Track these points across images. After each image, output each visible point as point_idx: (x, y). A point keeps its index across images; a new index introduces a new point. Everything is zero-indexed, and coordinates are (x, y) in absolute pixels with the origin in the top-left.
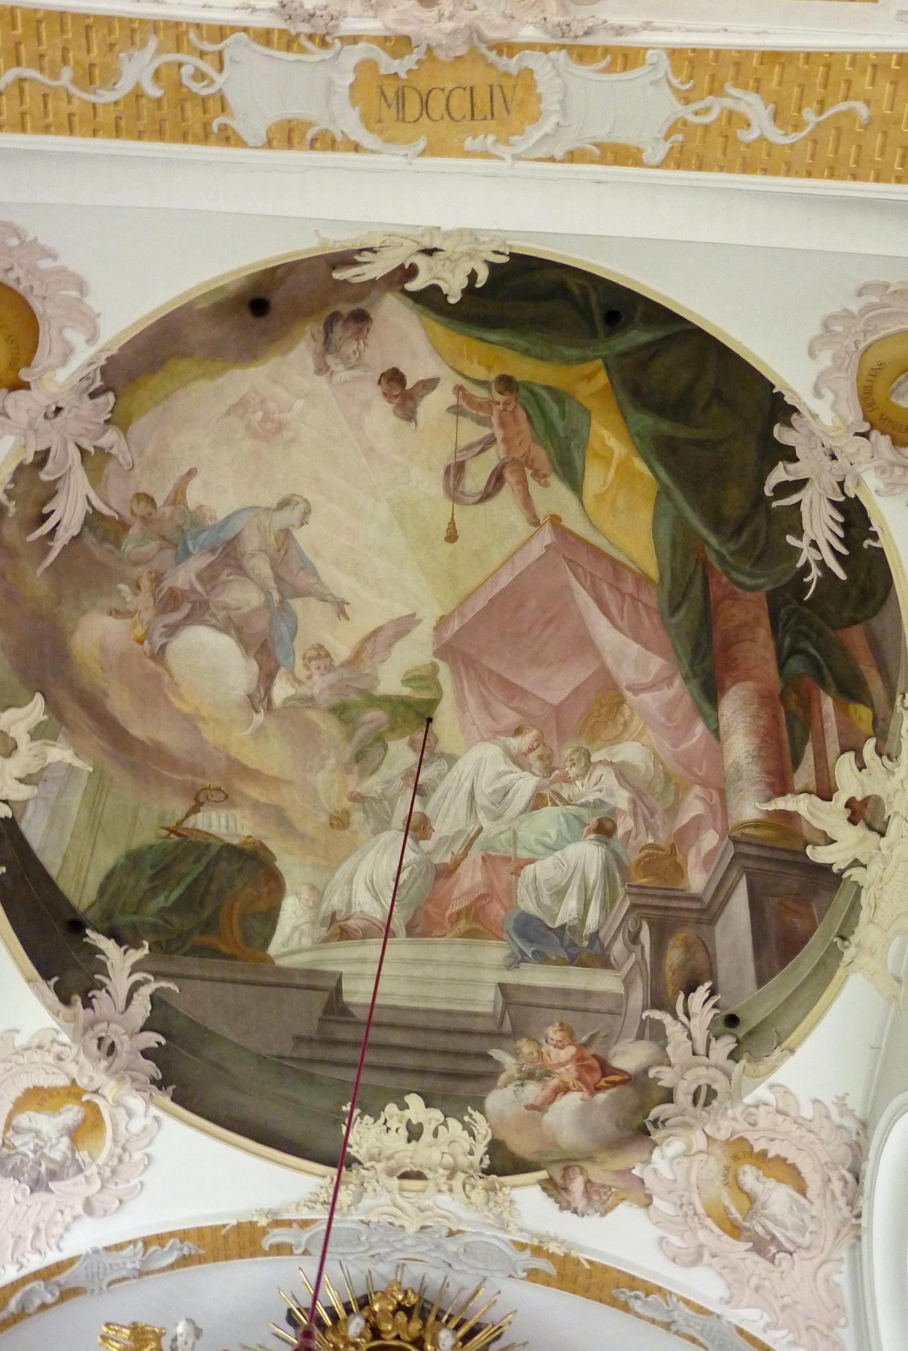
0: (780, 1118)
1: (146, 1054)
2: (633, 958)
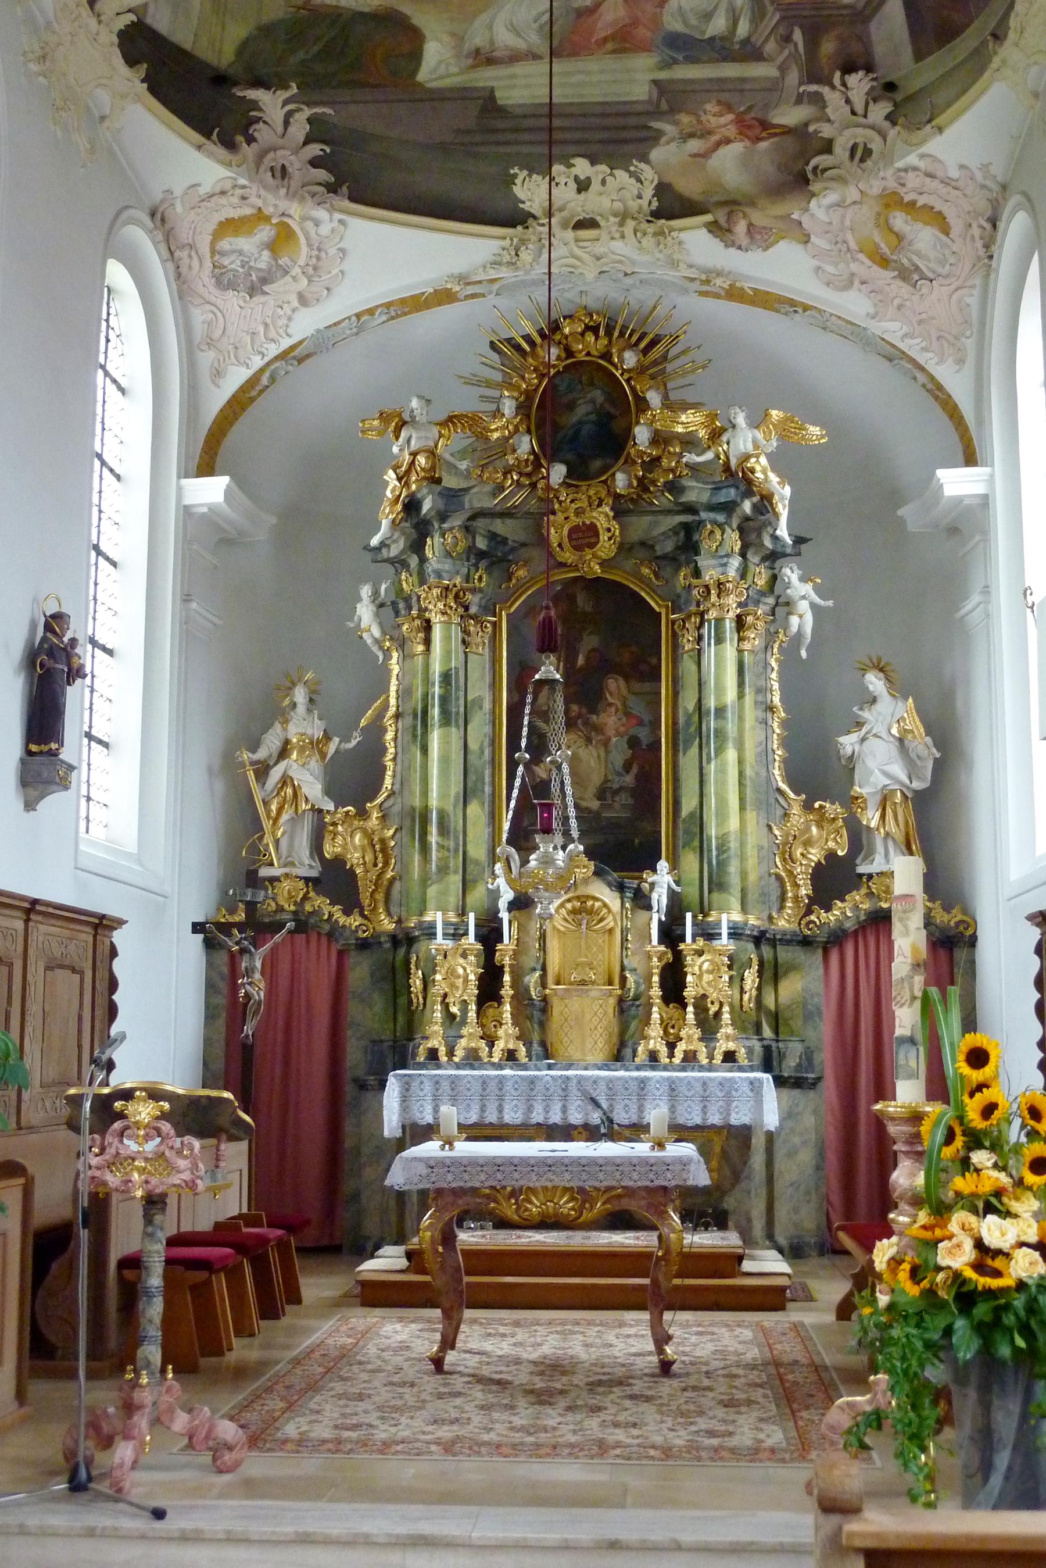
0: (928, 180)
1: (315, 163)
2: (786, 52)
